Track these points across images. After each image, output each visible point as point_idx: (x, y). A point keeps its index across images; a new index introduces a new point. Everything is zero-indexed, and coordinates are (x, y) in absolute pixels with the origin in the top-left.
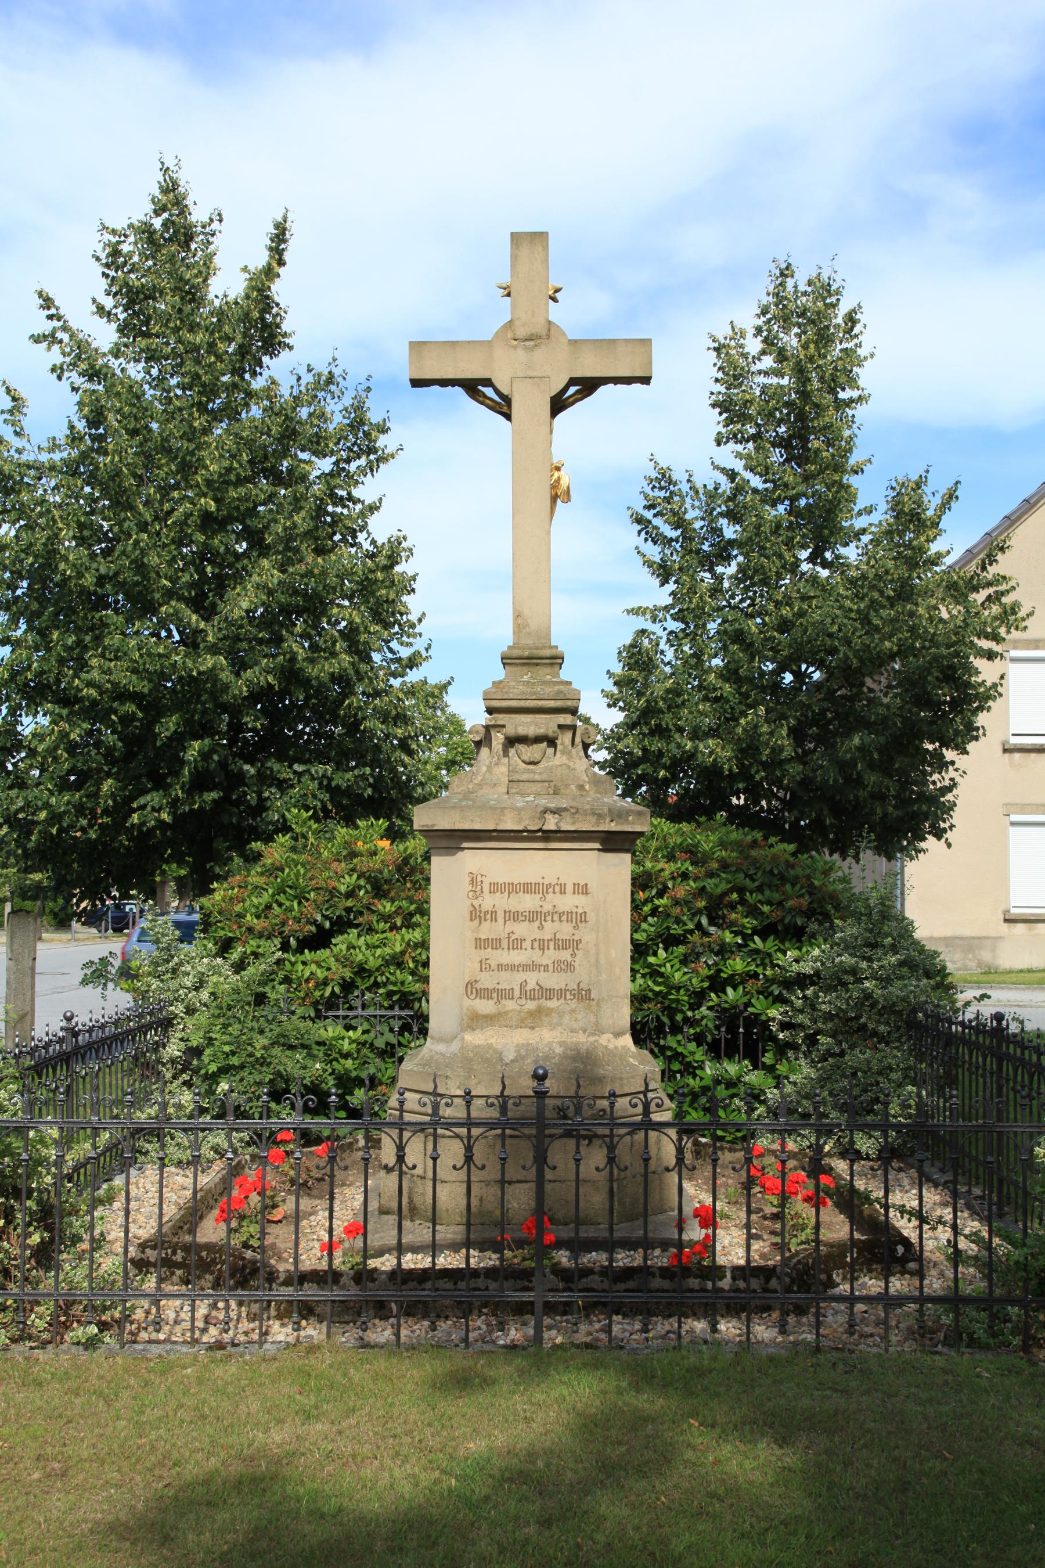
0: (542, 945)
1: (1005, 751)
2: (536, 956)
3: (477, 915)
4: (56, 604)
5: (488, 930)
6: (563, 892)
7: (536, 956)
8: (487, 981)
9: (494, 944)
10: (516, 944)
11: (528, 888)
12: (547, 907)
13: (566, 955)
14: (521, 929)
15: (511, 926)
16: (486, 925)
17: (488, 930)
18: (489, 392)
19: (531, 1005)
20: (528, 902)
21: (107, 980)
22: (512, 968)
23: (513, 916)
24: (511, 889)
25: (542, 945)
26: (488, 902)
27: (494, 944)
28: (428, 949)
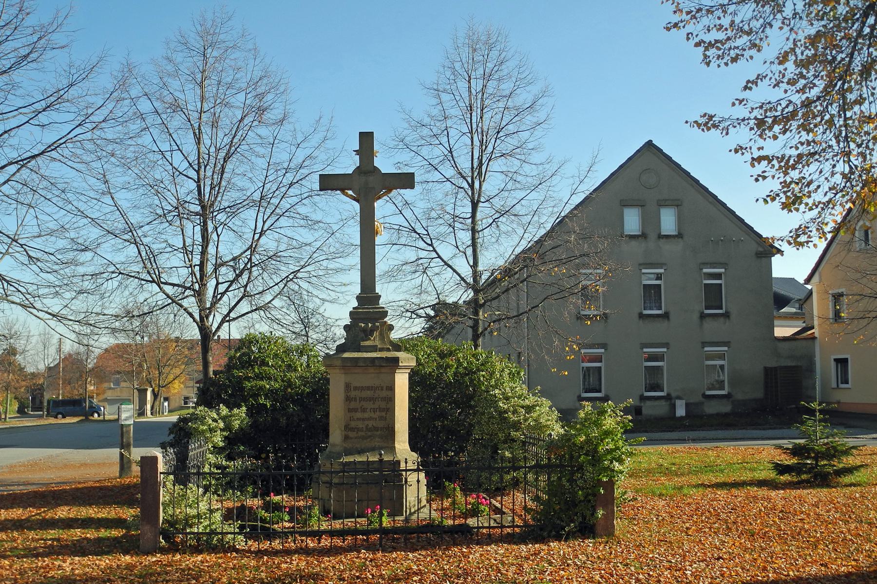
0: (374, 410)
1: (578, 318)
2: (372, 415)
3: (348, 399)
4: (852, 19)
5: (353, 405)
6: (382, 390)
7: (372, 415)
8: (353, 424)
9: (355, 410)
10: (364, 410)
11: (368, 388)
12: (376, 395)
13: (383, 414)
14: (365, 404)
15: (363, 403)
16: (353, 403)
17: (353, 405)
18: (51, 296)
19: (369, 434)
20: (369, 394)
21: (263, 496)
22: (364, 420)
23: (362, 399)
24: (362, 389)
25: (374, 410)
26: (353, 394)
27: (355, 410)
28: (541, 530)
